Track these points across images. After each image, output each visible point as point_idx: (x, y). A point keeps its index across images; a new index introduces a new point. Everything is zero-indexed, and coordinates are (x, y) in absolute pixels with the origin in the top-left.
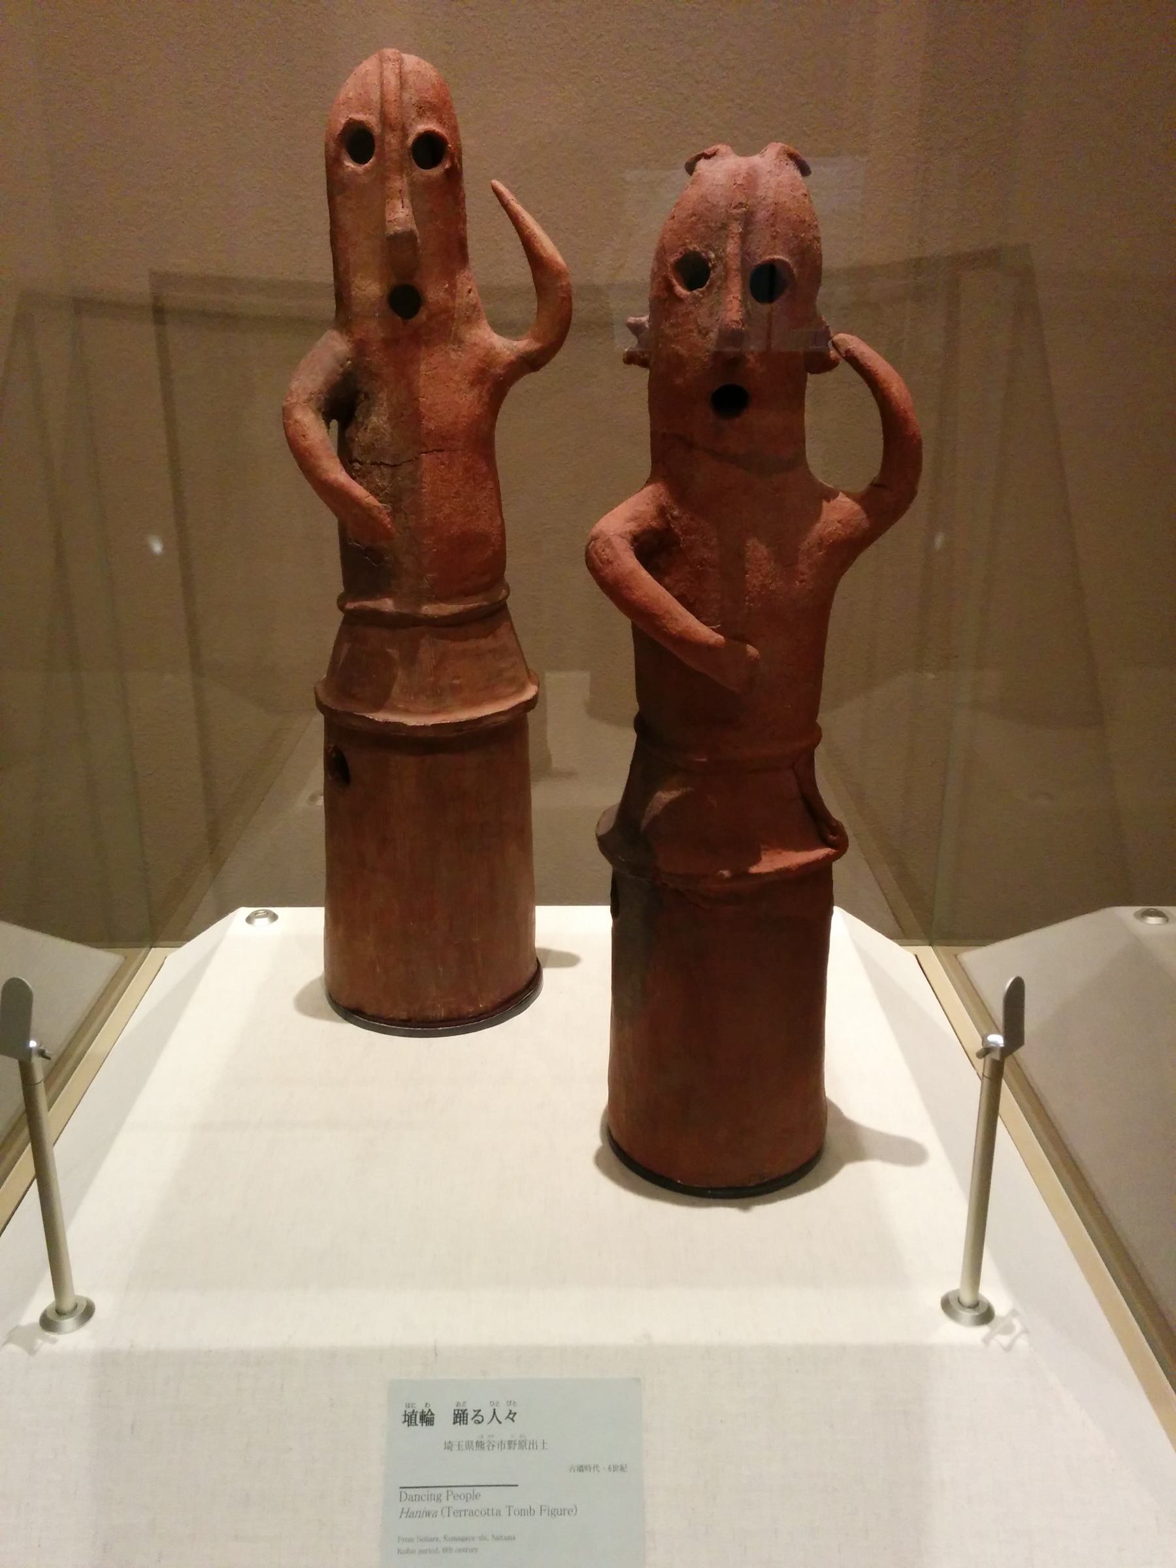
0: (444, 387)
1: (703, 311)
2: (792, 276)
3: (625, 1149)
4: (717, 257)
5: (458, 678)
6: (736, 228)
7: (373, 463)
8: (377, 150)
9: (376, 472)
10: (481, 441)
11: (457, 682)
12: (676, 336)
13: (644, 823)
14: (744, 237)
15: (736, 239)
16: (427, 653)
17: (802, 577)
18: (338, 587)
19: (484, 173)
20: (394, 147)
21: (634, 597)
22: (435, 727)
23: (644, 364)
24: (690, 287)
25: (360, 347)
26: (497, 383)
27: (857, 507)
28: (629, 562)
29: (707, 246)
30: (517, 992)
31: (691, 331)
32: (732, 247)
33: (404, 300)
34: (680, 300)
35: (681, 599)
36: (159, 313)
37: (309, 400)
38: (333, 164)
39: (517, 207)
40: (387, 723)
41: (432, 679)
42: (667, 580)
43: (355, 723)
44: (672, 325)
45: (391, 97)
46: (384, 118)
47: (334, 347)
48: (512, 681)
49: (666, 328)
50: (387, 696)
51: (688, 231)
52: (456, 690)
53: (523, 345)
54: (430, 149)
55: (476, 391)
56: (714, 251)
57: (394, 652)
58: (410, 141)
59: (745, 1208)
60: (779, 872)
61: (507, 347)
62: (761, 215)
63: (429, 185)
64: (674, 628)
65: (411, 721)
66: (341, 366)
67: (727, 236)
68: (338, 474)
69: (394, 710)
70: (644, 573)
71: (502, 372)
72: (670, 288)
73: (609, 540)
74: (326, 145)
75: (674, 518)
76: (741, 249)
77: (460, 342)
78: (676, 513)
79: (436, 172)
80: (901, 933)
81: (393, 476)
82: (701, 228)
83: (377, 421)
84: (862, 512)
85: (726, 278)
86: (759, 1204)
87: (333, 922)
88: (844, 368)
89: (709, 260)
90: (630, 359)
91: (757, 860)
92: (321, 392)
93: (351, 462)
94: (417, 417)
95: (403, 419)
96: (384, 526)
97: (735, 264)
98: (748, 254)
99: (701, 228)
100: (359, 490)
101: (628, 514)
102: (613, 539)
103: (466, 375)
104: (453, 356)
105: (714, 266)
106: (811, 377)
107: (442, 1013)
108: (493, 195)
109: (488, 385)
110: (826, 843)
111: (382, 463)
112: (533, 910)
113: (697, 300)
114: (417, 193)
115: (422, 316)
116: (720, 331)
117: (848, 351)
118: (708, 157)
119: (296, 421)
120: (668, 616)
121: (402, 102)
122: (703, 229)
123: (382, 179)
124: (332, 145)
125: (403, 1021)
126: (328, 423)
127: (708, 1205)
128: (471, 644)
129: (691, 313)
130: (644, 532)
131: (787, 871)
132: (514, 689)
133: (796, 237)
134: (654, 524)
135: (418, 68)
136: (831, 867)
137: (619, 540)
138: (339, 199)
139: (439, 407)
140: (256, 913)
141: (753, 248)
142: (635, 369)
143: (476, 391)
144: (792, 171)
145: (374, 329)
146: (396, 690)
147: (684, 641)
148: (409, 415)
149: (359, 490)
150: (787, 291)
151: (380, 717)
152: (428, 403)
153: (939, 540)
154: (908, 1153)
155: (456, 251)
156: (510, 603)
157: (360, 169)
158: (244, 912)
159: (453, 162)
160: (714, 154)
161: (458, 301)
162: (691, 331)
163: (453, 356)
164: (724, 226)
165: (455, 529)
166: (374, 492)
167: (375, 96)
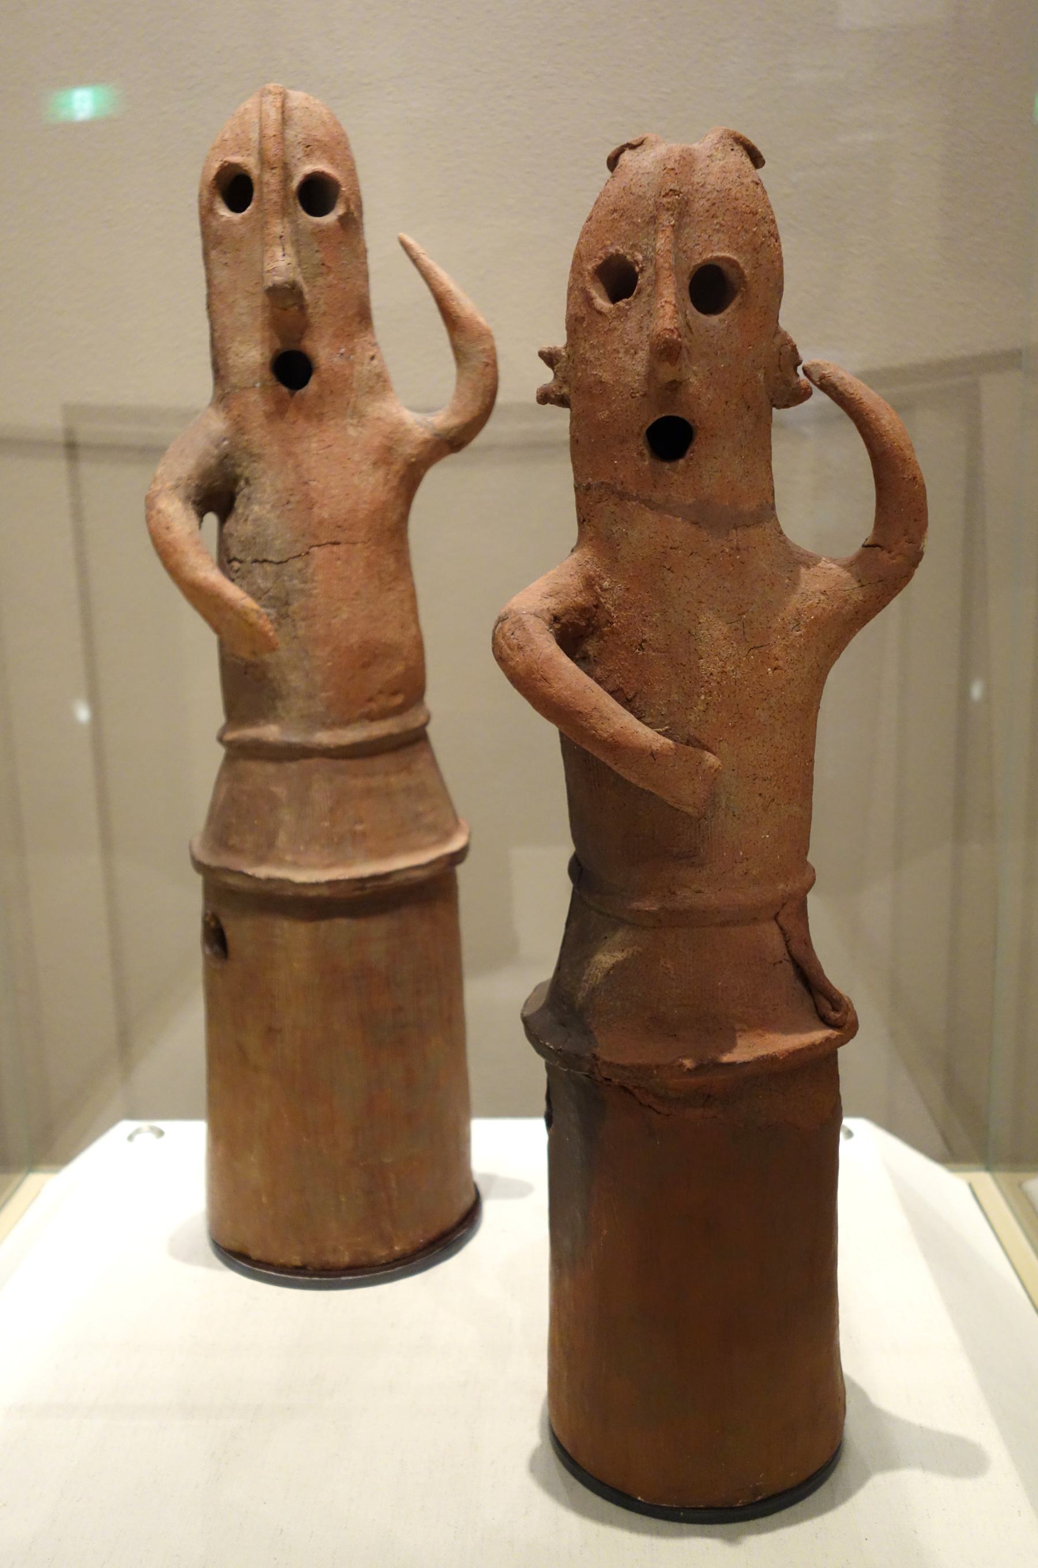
0: (333, 464)
1: (631, 325)
2: (742, 276)
3: (569, 1451)
4: (645, 258)
5: (361, 821)
6: (667, 220)
7: (256, 561)
8: (255, 195)
9: (257, 569)
11: (359, 828)
13: (581, 995)
14: (677, 229)
15: (668, 232)
16: (321, 793)
17: (775, 663)
18: (220, 719)
20: (273, 187)
21: (552, 691)
22: (330, 883)
23: (562, 401)
24: (614, 298)
25: (239, 427)
27: (846, 575)
28: (546, 646)
30: (448, 1228)
32: (662, 242)
33: (291, 369)
35: (616, 693)
36: (72, 448)
37: (177, 487)
38: (207, 213)
39: (427, 260)
40: (269, 880)
41: (326, 824)
42: (598, 672)
43: (232, 881)
44: (592, 347)
45: (270, 132)
46: (264, 161)
48: (432, 828)
49: (584, 348)
50: (271, 844)
52: (357, 838)
54: (317, 194)
55: (380, 473)
56: (642, 253)
57: (280, 791)
58: (295, 183)
59: (732, 1539)
60: (761, 1061)
62: (699, 205)
63: (320, 234)
64: (605, 730)
65: (301, 876)
66: (217, 446)
67: (656, 232)
68: (209, 574)
69: (280, 863)
70: (565, 660)
71: (415, 452)
72: (589, 300)
73: (520, 619)
74: (200, 196)
76: (675, 245)
77: (360, 416)
78: (606, 584)
79: (330, 219)
80: (951, 1153)
81: (278, 576)
83: (259, 509)
84: (853, 581)
85: (655, 283)
86: (751, 1533)
87: (218, 1135)
88: (819, 397)
89: (637, 262)
90: (545, 397)
91: (731, 1046)
93: (230, 561)
94: (309, 504)
95: (290, 506)
96: (264, 635)
97: (665, 262)
100: (233, 592)
101: (546, 589)
102: (525, 618)
103: (368, 454)
104: (352, 432)
107: (346, 1258)
108: (400, 248)
109: (396, 467)
110: (826, 1022)
111: (265, 561)
112: (466, 1124)
113: (622, 315)
116: (651, 345)
117: (823, 377)
118: (632, 147)
119: (159, 512)
120: (596, 714)
121: (283, 139)
122: (627, 228)
124: (205, 193)
125: (297, 1267)
126: (201, 515)
127: (680, 1535)
128: (377, 781)
130: (567, 611)
131: (772, 1059)
132: (434, 838)
135: (306, 104)
136: (835, 1054)
137: (533, 619)
138: (213, 254)
139: (334, 492)
140: (138, 1131)
143: (380, 473)
144: (739, 158)
145: (255, 402)
146: (282, 838)
147: (615, 746)
149: (233, 592)
150: (738, 299)
151: (263, 872)
152: (320, 486)
153: (977, 691)
154: (960, 1459)
156: (430, 730)
157: (236, 217)
158: (126, 1126)
159: (348, 207)
160: (641, 144)
161: (358, 368)
163: (352, 432)
164: (654, 219)
165: (354, 639)
167: (255, 136)
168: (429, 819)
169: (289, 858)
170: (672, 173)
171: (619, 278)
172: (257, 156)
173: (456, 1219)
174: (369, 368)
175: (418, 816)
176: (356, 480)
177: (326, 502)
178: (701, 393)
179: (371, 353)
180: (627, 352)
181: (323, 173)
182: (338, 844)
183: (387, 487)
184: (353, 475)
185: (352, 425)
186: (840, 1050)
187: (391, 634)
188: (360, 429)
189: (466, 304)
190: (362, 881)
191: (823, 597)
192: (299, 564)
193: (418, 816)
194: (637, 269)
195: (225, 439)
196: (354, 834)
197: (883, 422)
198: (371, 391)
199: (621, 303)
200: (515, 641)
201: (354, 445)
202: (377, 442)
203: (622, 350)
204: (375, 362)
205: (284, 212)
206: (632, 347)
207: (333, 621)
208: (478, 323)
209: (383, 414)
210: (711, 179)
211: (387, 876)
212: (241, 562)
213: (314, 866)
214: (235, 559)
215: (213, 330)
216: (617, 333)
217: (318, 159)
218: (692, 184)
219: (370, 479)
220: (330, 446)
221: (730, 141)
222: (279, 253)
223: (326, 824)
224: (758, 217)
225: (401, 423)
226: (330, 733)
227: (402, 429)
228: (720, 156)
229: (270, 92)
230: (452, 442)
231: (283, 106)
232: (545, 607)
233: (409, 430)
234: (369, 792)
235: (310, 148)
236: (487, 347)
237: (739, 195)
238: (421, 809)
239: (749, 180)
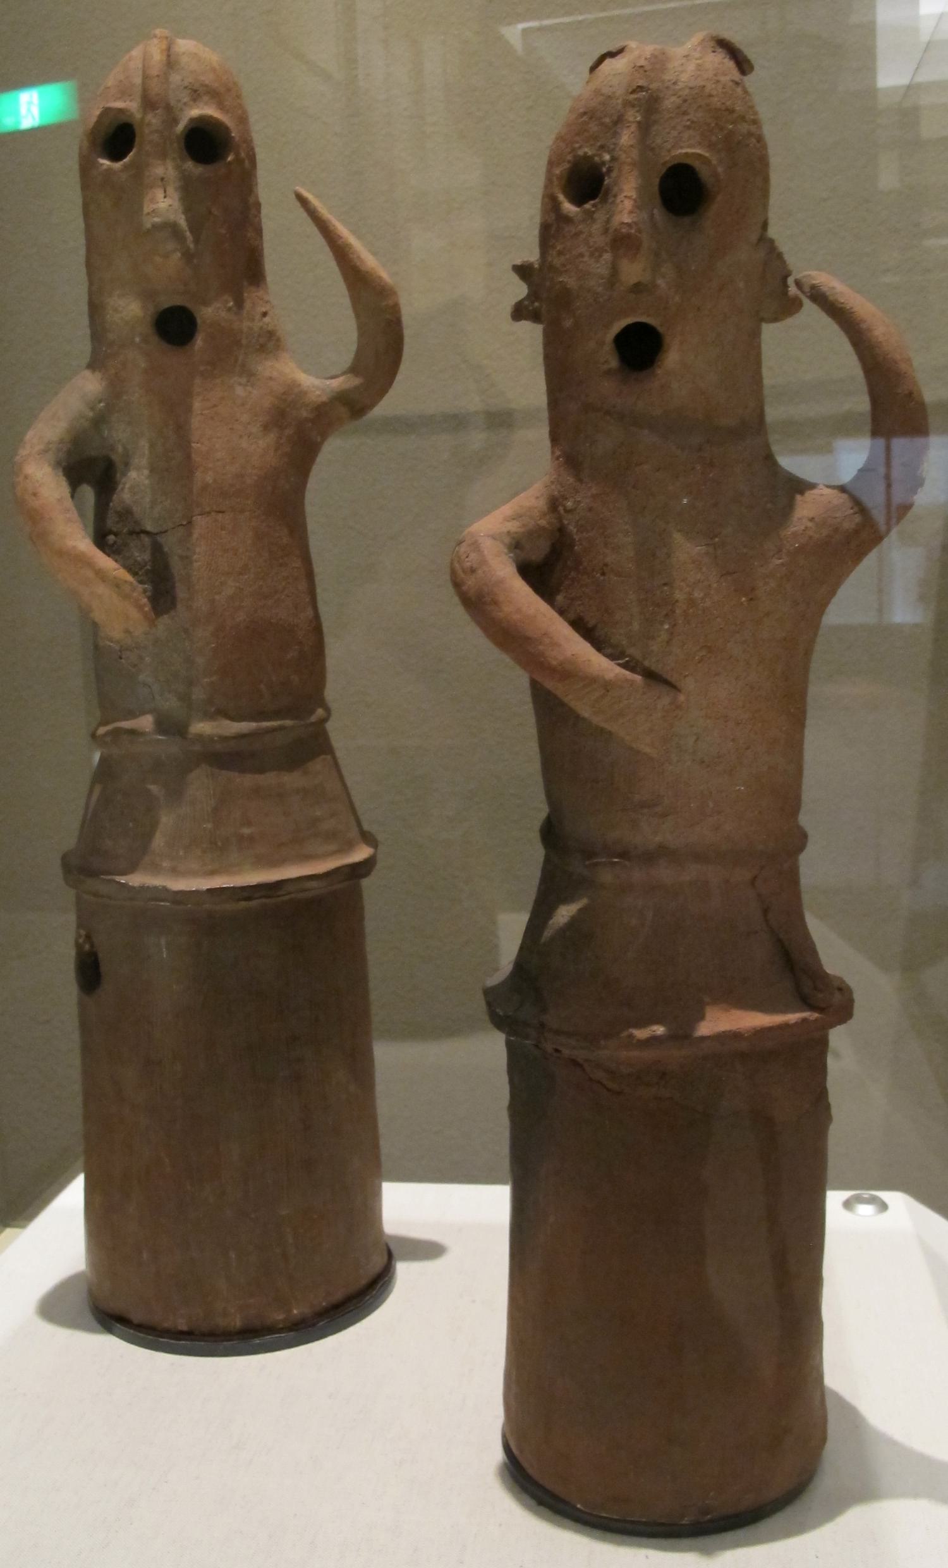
1: (597, 227)
5: (249, 824)
6: (634, 116)
10: (281, 503)
11: (246, 831)
12: (564, 265)
14: (645, 128)
24: (579, 201)
25: (115, 389)
26: (303, 432)
29: (602, 147)
31: (581, 255)
32: (626, 138)
34: (567, 219)
35: (579, 625)
37: (46, 451)
39: (343, 231)
40: (143, 889)
44: (560, 253)
46: (148, 103)
51: (578, 134)
54: (205, 143)
55: (271, 437)
56: (609, 152)
58: (180, 127)
62: (670, 102)
66: (92, 409)
69: (156, 869)
73: (476, 541)
75: (567, 511)
77: (251, 375)
78: (569, 504)
82: (594, 128)
88: (810, 310)
89: (603, 163)
92: (61, 441)
98: (652, 149)
99: (594, 128)
104: (240, 391)
105: (610, 170)
106: (770, 332)
107: (237, 1322)
109: (289, 432)
113: (590, 216)
114: (188, 189)
119: (26, 477)
122: (596, 129)
129: (581, 232)
133: (722, 129)
134: (543, 523)
141: (659, 141)
142: (515, 279)
143: (271, 437)
146: (159, 842)
151: (135, 880)
162: (581, 255)
163: (240, 391)
165: (241, 616)
167: (138, 80)
169: (166, 864)
170: (641, 71)
171: (585, 182)
172: (139, 100)
173: (364, 1282)
174: (261, 324)
176: (244, 444)
177: (210, 465)
179: (264, 310)
180: (592, 255)
181: (211, 117)
182: (218, 849)
183: (280, 452)
184: (241, 437)
185: (240, 384)
188: (249, 388)
189: (369, 260)
191: (810, 524)
194: (604, 170)
195: (100, 402)
196: (241, 838)
197: (876, 333)
198: (262, 349)
199: (587, 206)
200: (468, 564)
201: (243, 405)
203: (587, 254)
204: (267, 319)
206: (596, 250)
207: (217, 597)
208: (380, 277)
209: (275, 374)
210: (684, 77)
212: (116, 534)
213: (193, 874)
214: (111, 532)
215: (91, 284)
216: (583, 236)
217: (206, 104)
218: (663, 81)
219: (261, 442)
220: (215, 406)
221: (712, 43)
222: (159, 194)
223: (209, 826)
224: (735, 115)
225: (294, 385)
226: (214, 724)
227: (296, 390)
228: (697, 55)
229: (155, 36)
230: (352, 406)
231: (169, 49)
232: (505, 530)
233: (306, 393)
235: (196, 94)
236: (391, 302)
237: (714, 93)
238: (318, 813)
239: (728, 78)
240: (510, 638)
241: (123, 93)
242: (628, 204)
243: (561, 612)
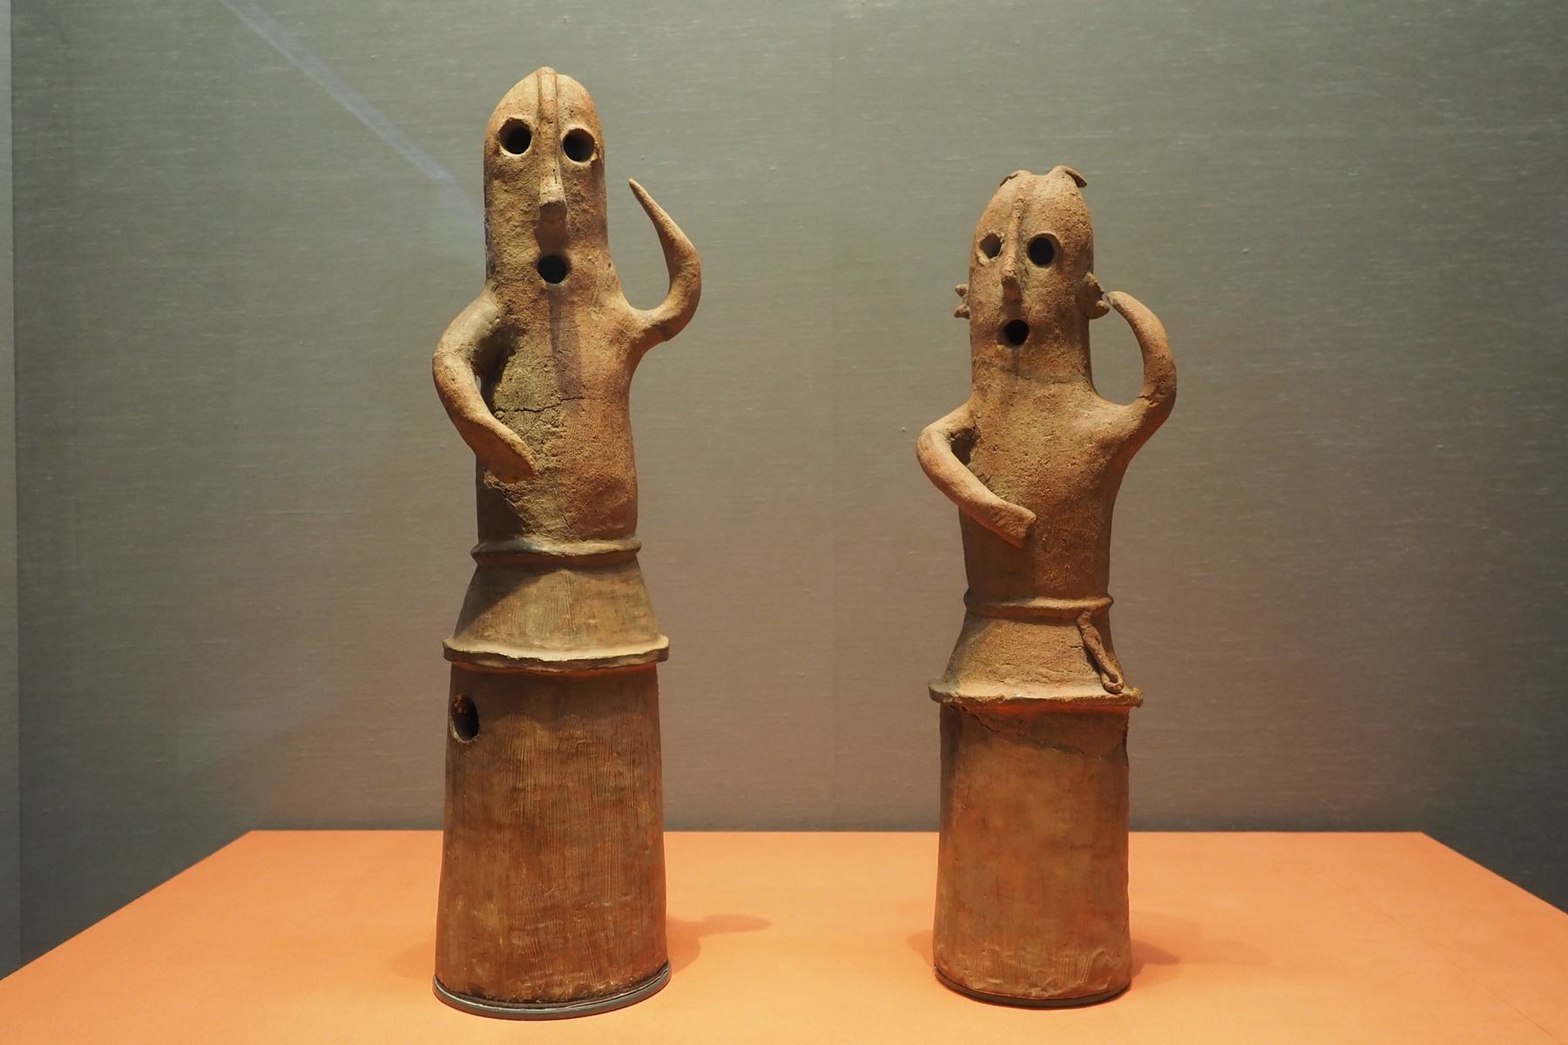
1: (996, 271)
6: (1016, 214)
10: (619, 393)
19: (621, 167)
26: (638, 346)
32: (1012, 226)
33: (552, 267)
39: (650, 199)
40: (522, 660)
45: (548, 98)
46: (542, 117)
47: (481, 313)
48: (645, 629)
53: (662, 311)
54: (577, 145)
55: (615, 349)
58: (562, 136)
61: (646, 317)
63: (577, 173)
65: (546, 657)
69: (530, 647)
77: (598, 304)
79: (585, 164)
83: (518, 372)
109: (626, 346)
113: (993, 265)
114: (568, 176)
115: (563, 284)
123: (534, 163)
124: (492, 140)
132: (646, 637)
145: (523, 293)
148: (562, 362)
149: (502, 429)
155: (597, 229)
163: (594, 316)
164: (1010, 215)
165: (593, 472)
166: (519, 432)
167: (534, 101)
168: (643, 621)
175: (635, 618)
178: (1034, 304)
182: (573, 631)
186: (1091, 322)
187: (618, 471)
189: (678, 232)
190: (595, 662)
192: (553, 413)
193: (635, 618)
196: (588, 626)
202: (612, 325)
205: (554, 153)
211: (615, 659)
222: (552, 180)
234: (599, 594)
240: (945, 486)
241: (522, 110)
242: (1010, 261)
243: (973, 471)
